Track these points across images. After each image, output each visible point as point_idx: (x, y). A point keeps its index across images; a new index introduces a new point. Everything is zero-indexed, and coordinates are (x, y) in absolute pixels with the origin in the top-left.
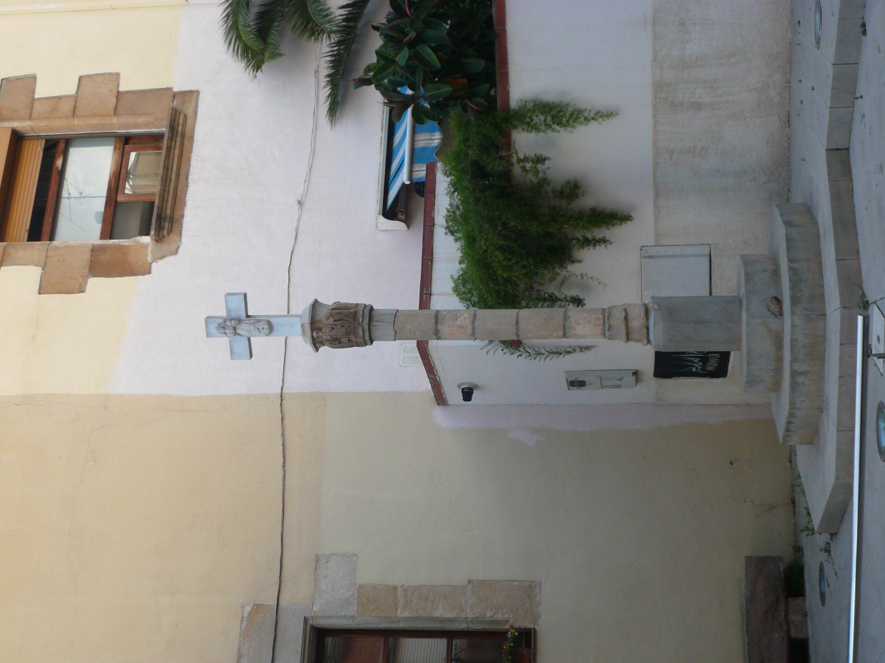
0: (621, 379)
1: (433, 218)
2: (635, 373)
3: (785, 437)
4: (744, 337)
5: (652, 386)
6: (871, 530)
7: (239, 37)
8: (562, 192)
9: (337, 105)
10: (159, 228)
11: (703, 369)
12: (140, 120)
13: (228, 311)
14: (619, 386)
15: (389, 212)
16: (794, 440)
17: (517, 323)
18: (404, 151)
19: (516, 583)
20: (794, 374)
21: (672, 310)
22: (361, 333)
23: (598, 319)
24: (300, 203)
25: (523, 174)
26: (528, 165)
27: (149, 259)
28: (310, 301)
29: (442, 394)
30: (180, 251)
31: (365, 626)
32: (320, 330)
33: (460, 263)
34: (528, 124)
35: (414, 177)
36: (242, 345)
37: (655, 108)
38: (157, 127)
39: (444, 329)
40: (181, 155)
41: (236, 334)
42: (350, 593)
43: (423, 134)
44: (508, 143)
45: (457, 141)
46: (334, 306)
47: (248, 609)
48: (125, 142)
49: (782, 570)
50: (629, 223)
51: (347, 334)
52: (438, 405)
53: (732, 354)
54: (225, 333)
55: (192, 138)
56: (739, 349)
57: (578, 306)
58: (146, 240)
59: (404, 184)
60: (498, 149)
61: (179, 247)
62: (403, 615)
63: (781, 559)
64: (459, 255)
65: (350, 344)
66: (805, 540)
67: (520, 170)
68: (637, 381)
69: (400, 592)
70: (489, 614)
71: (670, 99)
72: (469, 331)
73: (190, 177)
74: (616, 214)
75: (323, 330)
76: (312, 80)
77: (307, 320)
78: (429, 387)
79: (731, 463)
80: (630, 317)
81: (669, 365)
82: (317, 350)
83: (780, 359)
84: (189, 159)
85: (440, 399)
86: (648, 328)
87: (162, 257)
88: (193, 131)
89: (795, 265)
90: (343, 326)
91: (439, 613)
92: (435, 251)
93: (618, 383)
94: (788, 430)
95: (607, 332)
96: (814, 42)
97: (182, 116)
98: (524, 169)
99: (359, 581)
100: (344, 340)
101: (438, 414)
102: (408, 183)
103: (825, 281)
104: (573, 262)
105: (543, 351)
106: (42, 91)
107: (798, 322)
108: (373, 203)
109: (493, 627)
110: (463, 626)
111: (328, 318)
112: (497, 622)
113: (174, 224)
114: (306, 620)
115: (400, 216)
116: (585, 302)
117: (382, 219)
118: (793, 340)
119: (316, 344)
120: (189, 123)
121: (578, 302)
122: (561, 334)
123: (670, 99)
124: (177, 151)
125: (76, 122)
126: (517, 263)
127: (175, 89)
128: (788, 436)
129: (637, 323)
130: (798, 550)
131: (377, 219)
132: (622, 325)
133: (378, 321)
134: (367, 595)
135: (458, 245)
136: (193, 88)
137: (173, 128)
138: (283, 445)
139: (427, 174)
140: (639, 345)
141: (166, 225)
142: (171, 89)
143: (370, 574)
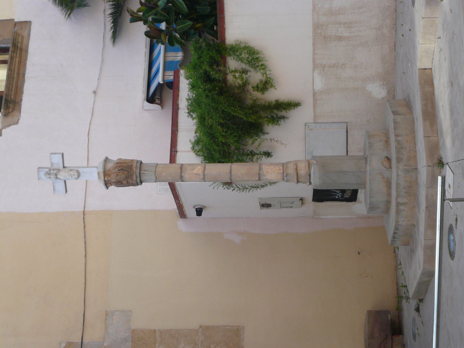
0: (293, 203)
1: (178, 105)
2: (301, 199)
3: (393, 241)
4: (368, 181)
6: (443, 300)
8: (257, 87)
11: (342, 197)
13: (52, 164)
14: (291, 207)
15: (151, 99)
16: (398, 243)
17: (231, 172)
18: (160, 62)
19: (229, 328)
20: (398, 204)
21: (324, 163)
22: (135, 178)
23: (280, 170)
24: (95, 92)
25: (234, 79)
26: (237, 75)
28: (103, 158)
29: (183, 212)
30: (20, 121)
32: (109, 176)
33: (195, 133)
34: (238, 56)
35: (165, 79)
36: (60, 186)
37: (314, 39)
38: (4, 44)
40: (20, 62)
41: (57, 178)
42: (127, 334)
43: (171, 53)
45: (193, 56)
46: (118, 161)
49: (389, 319)
50: (299, 107)
51: (126, 178)
52: (181, 218)
54: (50, 178)
55: (27, 51)
56: (365, 188)
57: (268, 157)
59: (159, 83)
60: (218, 66)
61: (19, 119)
63: (389, 312)
64: (195, 127)
65: (128, 184)
67: (232, 77)
68: (302, 203)
69: (158, 333)
71: (323, 34)
72: (202, 177)
73: (26, 76)
74: (291, 103)
75: (112, 176)
77: (101, 170)
78: (175, 207)
79: (359, 253)
80: (299, 168)
81: (321, 196)
82: (107, 188)
83: (389, 195)
84: (25, 64)
85: (182, 214)
86: (310, 175)
87: (8, 126)
88: (27, 46)
89: (399, 139)
90: (124, 174)
92: (179, 124)
93: (291, 205)
94: (394, 237)
95: (285, 179)
96: (411, 3)
97: (20, 37)
99: (133, 327)
100: (125, 182)
101: (181, 223)
102: (162, 82)
103: (417, 148)
104: (264, 134)
105: (247, 187)
107: (400, 173)
111: (115, 168)
113: (16, 105)
115: (157, 101)
116: (272, 154)
118: (398, 184)
119: (107, 184)
120: (25, 41)
121: (268, 154)
122: (257, 178)
123: (323, 34)
124: (17, 59)
126: (231, 134)
127: (16, 20)
128: (394, 241)
129: (303, 171)
130: (399, 309)
131: (143, 104)
133: (145, 171)
135: (195, 121)
136: (27, 20)
137: (15, 45)
138: (85, 243)
139: (174, 78)
140: (305, 185)
141: (11, 106)
142: (13, 20)
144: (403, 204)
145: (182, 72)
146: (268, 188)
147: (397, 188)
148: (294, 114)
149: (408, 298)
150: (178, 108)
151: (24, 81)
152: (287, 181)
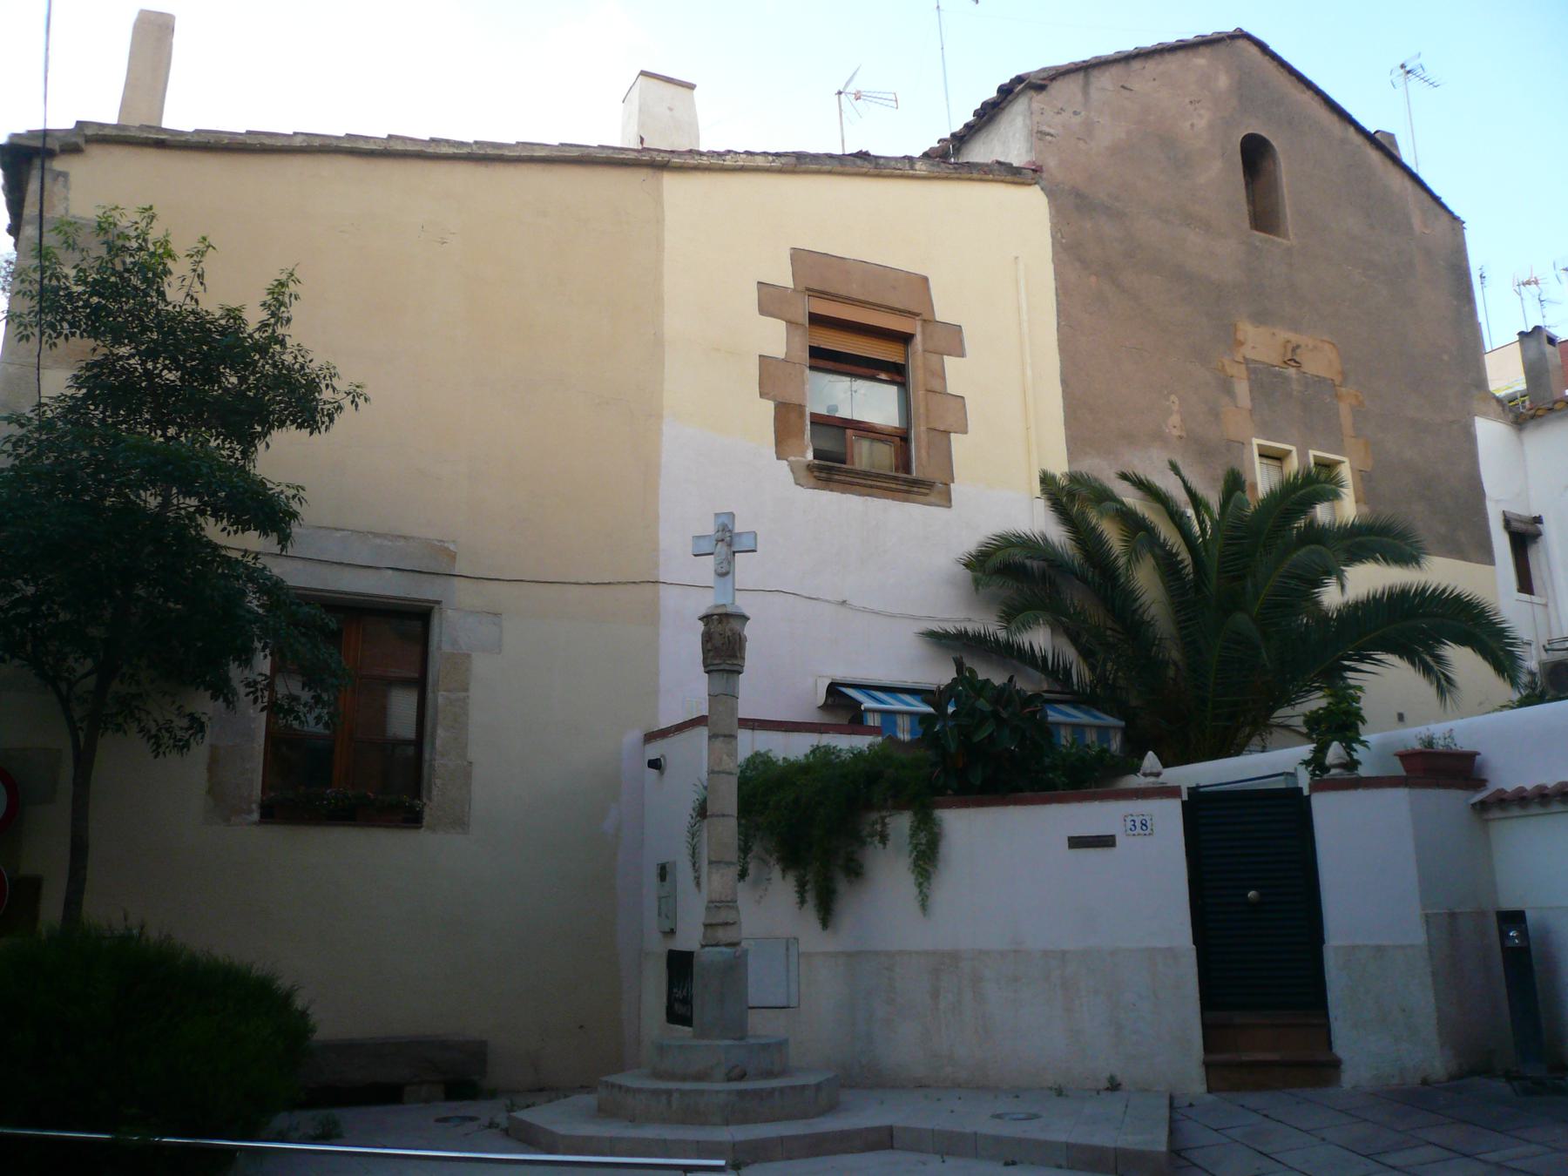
2: (672, 932)
5: (658, 947)
7: (999, 548)
9: (938, 639)
10: (820, 468)
12: (923, 453)
13: (740, 534)
15: (834, 689)
20: (669, 1093)
21: (734, 969)
26: (878, 827)
27: (792, 458)
28: (747, 614)
39: (719, 743)
47: (452, 547)
55: (907, 500)
58: (810, 456)
62: (440, 697)
64: (792, 758)
65: (705, 652)
69: (462, 695)
70: (438, 782)
76: (962, 615)
77: (730, 610)
81: (680, 965)
83: (684, 1078)
85: (651, 737)
86: (717, 945)
90: (723, 644)
91: (440, 732)
94: (613, 1086)
98: (874, 823)
100: (709, 646)
101: (636, 735)
106: (949, 361)
108: (843, 673)
110: (427, 756)
112: (430, 792)
114: (438, 602)
117: (827, 682)
118: (702, 1092)
119: (706, 619)
121: (743, 875)
125: (921, 393)
129: (722, 935)
130: (492, 1094)
134: (461, 662)
143: (481, 666)
144: (669, 1102)
145: (880, 739)
146: (690, 874)
147: (696, 1091)
148: (811, 914)
149: (510, 1110)
150: (821, 733)
151: (861, 495)
152: (708, 908)
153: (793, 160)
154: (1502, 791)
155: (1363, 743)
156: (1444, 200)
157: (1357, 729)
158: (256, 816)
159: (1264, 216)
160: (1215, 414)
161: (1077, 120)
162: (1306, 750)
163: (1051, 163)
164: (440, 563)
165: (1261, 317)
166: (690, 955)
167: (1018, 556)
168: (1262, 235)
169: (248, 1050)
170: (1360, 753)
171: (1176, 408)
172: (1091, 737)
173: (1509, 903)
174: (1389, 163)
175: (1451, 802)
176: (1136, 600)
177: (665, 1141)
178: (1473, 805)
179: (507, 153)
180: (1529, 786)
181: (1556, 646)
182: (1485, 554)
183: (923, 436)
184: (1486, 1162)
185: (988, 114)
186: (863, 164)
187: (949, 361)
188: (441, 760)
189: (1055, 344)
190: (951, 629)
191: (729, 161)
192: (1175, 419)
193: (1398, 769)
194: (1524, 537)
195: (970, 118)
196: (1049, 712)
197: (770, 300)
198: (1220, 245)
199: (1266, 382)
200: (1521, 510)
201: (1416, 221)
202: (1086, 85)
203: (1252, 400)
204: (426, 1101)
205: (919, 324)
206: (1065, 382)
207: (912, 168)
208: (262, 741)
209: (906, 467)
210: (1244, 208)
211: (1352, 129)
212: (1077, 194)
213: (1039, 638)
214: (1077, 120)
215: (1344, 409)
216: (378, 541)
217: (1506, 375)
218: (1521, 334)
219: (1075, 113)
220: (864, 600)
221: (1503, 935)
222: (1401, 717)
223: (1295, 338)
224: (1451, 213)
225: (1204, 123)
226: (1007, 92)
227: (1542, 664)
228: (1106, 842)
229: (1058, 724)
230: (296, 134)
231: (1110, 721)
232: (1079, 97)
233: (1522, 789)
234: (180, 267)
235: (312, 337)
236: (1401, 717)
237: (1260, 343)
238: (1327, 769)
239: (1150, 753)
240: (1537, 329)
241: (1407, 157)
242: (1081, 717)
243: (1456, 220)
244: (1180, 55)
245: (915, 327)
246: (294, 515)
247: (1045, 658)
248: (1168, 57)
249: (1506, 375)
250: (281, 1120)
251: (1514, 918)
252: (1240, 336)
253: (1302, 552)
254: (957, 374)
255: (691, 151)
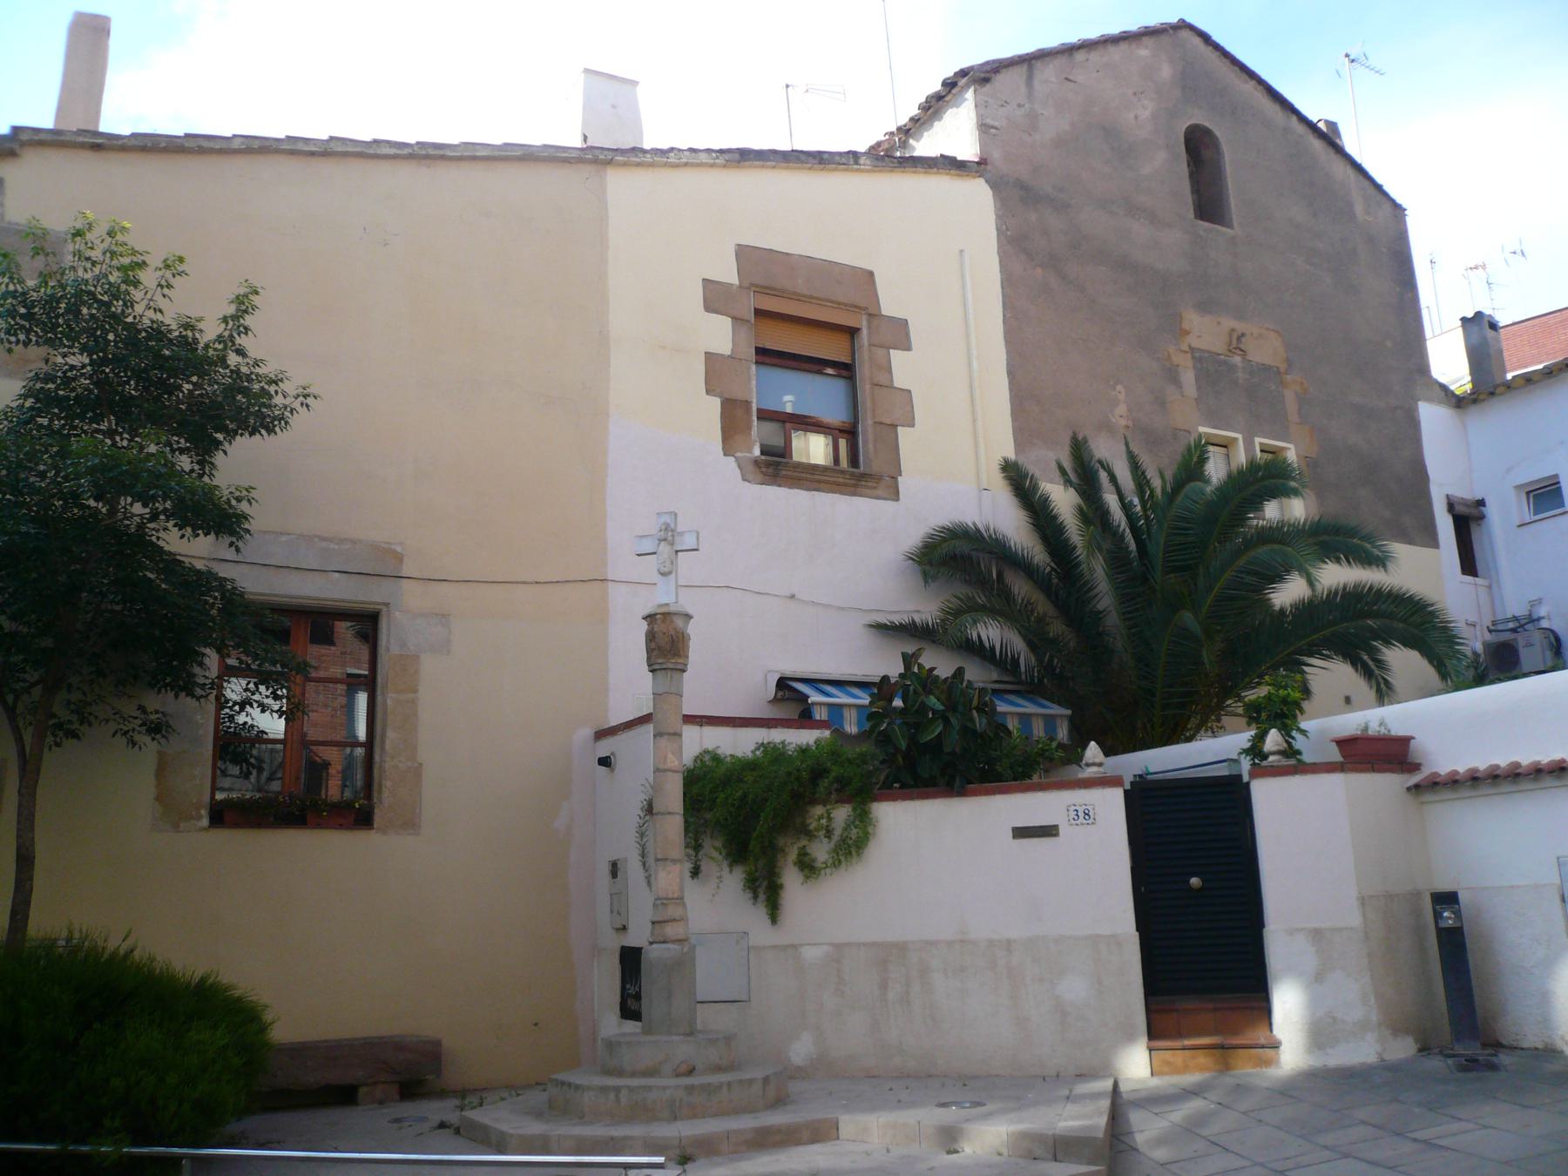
2: (624, 928)
5: (614, 943)
7: (944, 540)
9: (887, 630)
10: (768, 464)
12: (871, 446)
13: (681, 534)
15: (783, 683)
20: (617, 1089)
21: (683, 965)
24: (793, 596)
26: (824, 822)
28: (691, 612)
31: (379, 666)
36: (648, 546)
39: (663, 741)
44: (841, 801)
45: (852, 751)
47: (399, 549)
48: (850, 432)
53: (639, 1024)
58: (757, 452)
62: (389, 699)
64: (740, 755)
65: (649, 651)
66: (453, 1102)
68: (617, 930)
69: (411, 696)
70: (388, 784)
72: (661, 767)
76: (910, 607)
77: (672, 609)
78: (613, 723)
81: (631, 960)
83: (633, 1074)
85: (601, 734)
89: (725, 1089)
90: (666, 644)
91: (390, 734)
94: (563, 1083)
98: (821, 817)
100: (653, 645)
101: (587, 732)
106: (896, 356)
107: (668, 1092)
108: (792, 667)
109: (375, 787)
110: (377, 758)
112: (380, 792)
114: (387, 605)
118: (649, 1088)
119: (650, 618)
121: (695, 872)
125: (868, 387)
129: (671, 931)
130: (442, 1094)
132: (667, 911)
134: (410, 662)
137: (863, 476)
141: (770, 470)
143: (429, 666)
144: (617, 1097)
145: (827, 733)
148: (760, 913)
152: (655, 905)
153: (737, 156)
154: (1436, 774)
155: (1304, 732)
156: (1386, 188)
157: (1295, 717)
158: (205, 822)
159: (1209, 202)
160: (1161, 402)
161: (1021, 112)
162: (1243, 738)
163: (996, 155)
164: (387, 565)
165: (1205, 307)
166: (639, 949)
167: (962, 547)
168: (1206, 224)
169: (203, 1057)
170: (1299, 742)
171: (1122, 397)
172: (1038, 730)
173: (1444, 886)
174: (1331, 152)
175: (1387, 785)
176: (1091, 589)
177: (612, 1138)
178: (1409, 789)
179: (449, 153)
180: (1462, 768)
181: (1500, 627)
182: (1432, 540)
183: (870, 430)
184: (1415, 1140)
185: (934, 106)
186: (820, 160)
187: (896, 356)
188: (390, 762)
189: (1001, 335)
190: (897, 619)
191: (672, 158)
192: (1122, 409)
193: (1335, 755)
194: (1467, 519)
195: (915, 111)
196: (997, 702)
197: (715, 297)
198: (1168, 237)
199: (1212, 371)
200: (1464, 492)
201: (1359, 208)
202: (1030, 78)
203: (1198, 389)
204: (381, 1103)
205: (864, 318)
206: (1011, 373)
207: (856, 163)
208: (210, 747)
209: (854, 460)
210: (1188, 198)
211: (1294, 118)
212: (1022, 186)
213: (991, 632)
214: (1021, 112)
215: (1289, 396)
216: (324, 544)
217: (1449, 362)
218: (1464, 320)
219: (1019, 105)
220: (801, 594)
221: (1437, 916)
222: (1348, 700)
223: (1240, 326)
224: (1393, 201)
225: (1146, 113)
226: (950, 85)
227: (1486, 645)
228: (1049, 831)
229: (1006, 713)
230: (235, 136)
231: (1056, 710)
232: (1023, 89)
233: (1455, 772)
234: (148, 278)
235: (271, 347)
236: (1348, 700)
237: (1206, 332)
238: (1265, 757)
239: (1093, 743)
240: (1479, 314)
241: (1351, 148)
242: (1030, 708)
243: (1398, 210)
244: (1123, 46)
245: (863, 323)
246: (245, 517)
247: (993, 649)
248: (1111, 49)
249: (1449, 362)
250: (233, 1127)
251: (1446, 899)
252: (1186, 326)
253: (1266, 548)
254: (904, 368)
255: (634, 150)
